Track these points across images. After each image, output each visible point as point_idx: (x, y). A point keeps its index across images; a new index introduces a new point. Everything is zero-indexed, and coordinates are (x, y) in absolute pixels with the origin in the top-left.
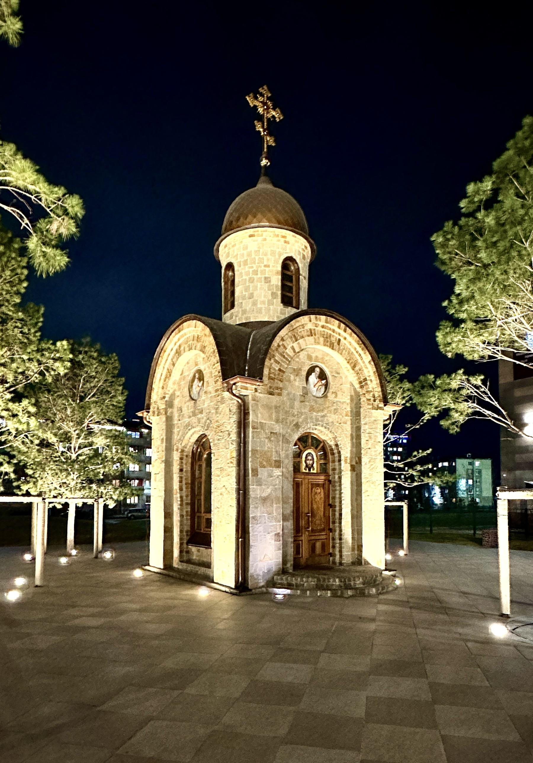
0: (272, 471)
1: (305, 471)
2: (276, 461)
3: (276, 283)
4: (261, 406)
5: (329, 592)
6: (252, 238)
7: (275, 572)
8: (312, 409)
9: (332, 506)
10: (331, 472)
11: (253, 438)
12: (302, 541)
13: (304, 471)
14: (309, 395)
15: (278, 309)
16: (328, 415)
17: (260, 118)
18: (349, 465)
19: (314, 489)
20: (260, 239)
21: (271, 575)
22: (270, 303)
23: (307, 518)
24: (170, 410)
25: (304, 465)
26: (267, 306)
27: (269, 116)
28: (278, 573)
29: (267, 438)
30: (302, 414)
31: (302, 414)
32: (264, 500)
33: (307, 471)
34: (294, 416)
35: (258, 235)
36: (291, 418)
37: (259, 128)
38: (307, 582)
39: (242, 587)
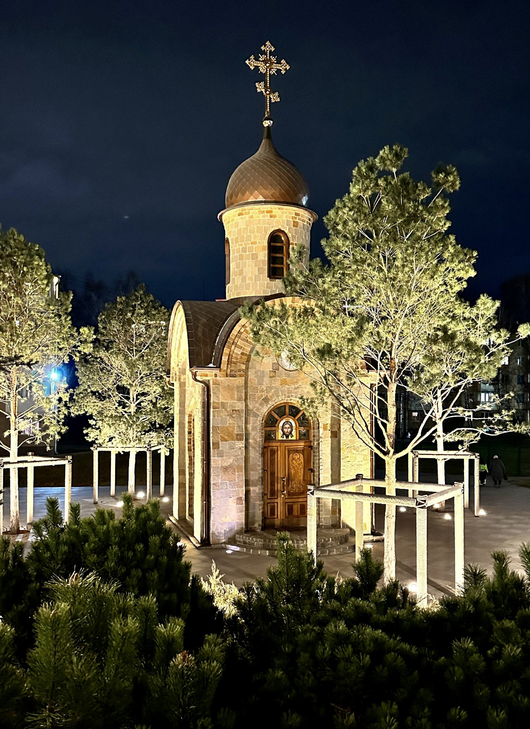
0: (235, 443)
1: (282, 439)
2: (237, 435)
3: (263, 258)
4: (222, 388)
5: (267, 551)
6: (241, 216)
7: (237, 531)
8: (284, 382)
9: (312, 471)
10: (312, 439)
11: (214, 416)
12: (277, 503)
13: (280, 438)
14: (280, 369)
15: (265, 283)
16: (303, 386)
17: (261, 77)
18: (330, 432)
19: (291, 455)
20: (247, 216)
21: (232, 534)
22: (257, 278)
23: (282, 482)
24: (183, 377)
25: (280, 432)
26: (254, 281)
27: (273, 71)
28: (240, 532)
29: (228, 415)
30: (271, 388)
31: (271, 388)
32: (226, 469)
33: (285, 438)
34: (263, 391)
35: (246, 214)
36: (259, 394)
37: (260, 87)
38: (256, 541)
39: (205, 542)
